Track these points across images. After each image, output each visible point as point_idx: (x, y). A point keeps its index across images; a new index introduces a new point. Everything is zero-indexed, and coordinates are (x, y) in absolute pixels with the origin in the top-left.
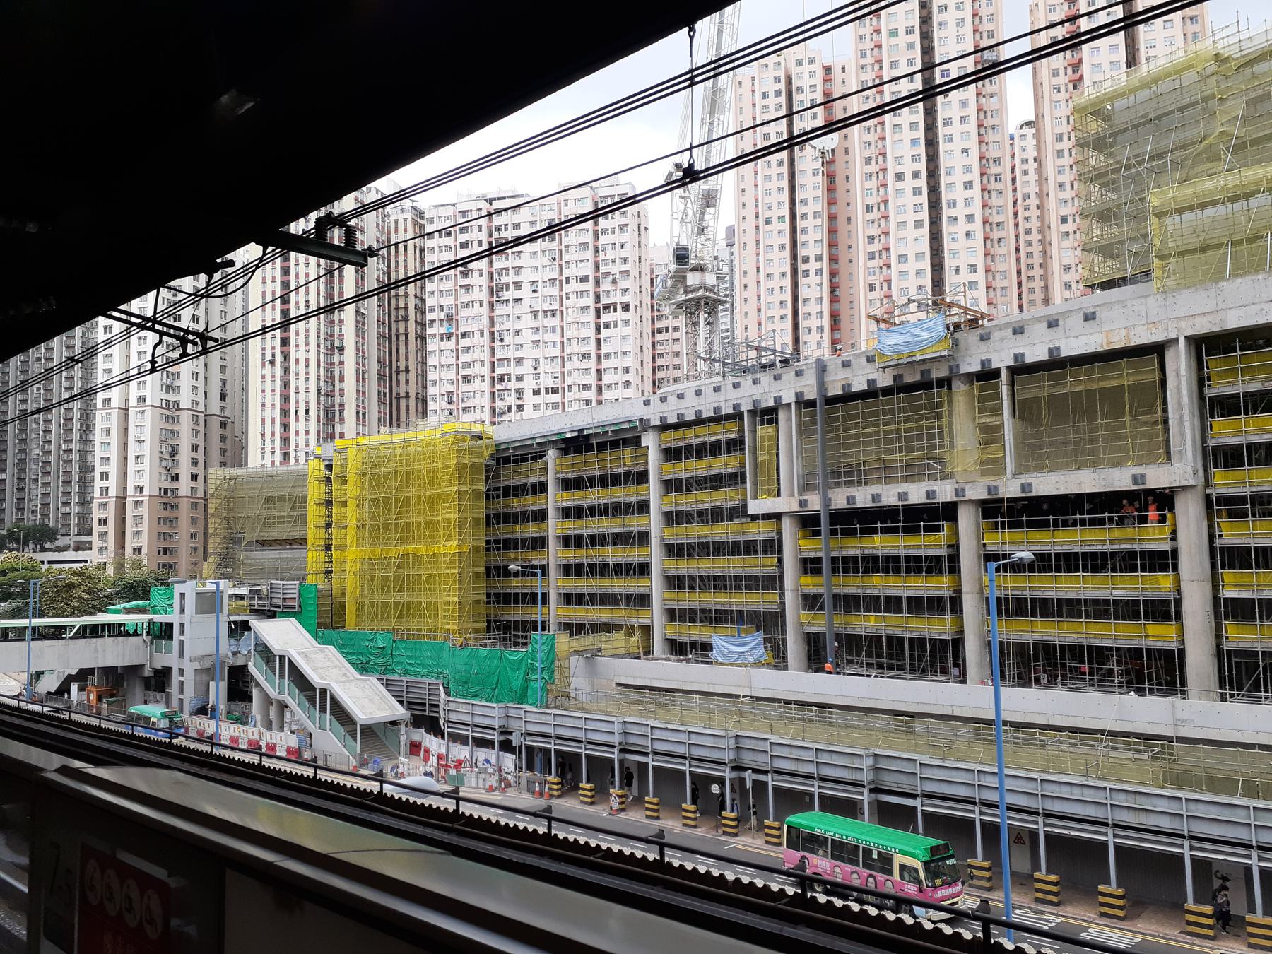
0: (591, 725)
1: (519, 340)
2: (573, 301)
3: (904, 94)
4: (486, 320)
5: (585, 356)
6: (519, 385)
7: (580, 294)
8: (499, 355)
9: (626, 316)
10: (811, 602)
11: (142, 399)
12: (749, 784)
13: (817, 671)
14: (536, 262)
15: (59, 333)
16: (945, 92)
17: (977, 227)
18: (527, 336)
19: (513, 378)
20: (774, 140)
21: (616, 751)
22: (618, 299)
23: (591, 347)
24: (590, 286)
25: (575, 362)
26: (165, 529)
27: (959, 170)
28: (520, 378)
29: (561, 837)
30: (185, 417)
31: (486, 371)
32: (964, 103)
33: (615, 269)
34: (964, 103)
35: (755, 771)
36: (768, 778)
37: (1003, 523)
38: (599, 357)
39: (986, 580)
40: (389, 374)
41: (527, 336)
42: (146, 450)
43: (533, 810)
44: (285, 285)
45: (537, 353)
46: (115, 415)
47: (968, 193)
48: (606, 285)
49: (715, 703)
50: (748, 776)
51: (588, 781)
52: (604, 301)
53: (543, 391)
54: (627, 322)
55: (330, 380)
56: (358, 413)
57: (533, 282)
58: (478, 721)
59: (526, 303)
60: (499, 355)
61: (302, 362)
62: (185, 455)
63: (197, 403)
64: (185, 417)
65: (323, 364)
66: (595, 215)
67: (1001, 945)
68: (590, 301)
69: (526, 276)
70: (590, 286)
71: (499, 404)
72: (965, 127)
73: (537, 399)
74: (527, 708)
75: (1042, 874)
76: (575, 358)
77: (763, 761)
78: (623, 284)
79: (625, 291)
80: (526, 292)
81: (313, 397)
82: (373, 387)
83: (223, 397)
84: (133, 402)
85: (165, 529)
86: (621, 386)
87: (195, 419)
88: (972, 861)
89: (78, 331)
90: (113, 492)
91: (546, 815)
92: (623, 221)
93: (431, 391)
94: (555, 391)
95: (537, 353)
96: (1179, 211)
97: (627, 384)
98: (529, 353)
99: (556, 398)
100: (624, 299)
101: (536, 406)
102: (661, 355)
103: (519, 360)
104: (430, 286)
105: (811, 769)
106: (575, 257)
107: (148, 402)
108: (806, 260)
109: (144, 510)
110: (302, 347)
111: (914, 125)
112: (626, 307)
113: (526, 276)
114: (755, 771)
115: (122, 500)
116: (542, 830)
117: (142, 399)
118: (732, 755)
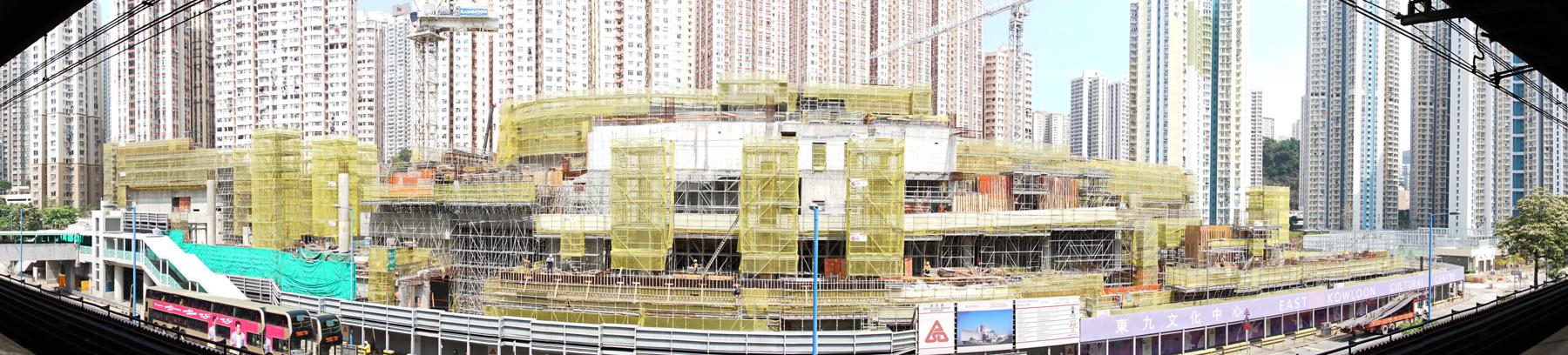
2: (310, 42)
5: (317, 76)
8: (260, 74)
22: (339, 40)
23: (321, 69)
24: (321, 32)
25: (309, 79)
31: (252, 84)
33: (337, 23)
36: (529, 345)
39: (995, 39)
40: (192, 88)
42: (56, 138)
48: (332, 32)
52: (331, 41)
55: (157, 93)
60: (260, 74)
62: (75, 139)
68: (321, 41)
70: (321, 32)
71: (261, 106)
78: (343, 31)
82: (182, 95)
83: (96, 106)
93: (217, 97)
99: (298, 101)
109: (56, 172)
112: (344, 46)
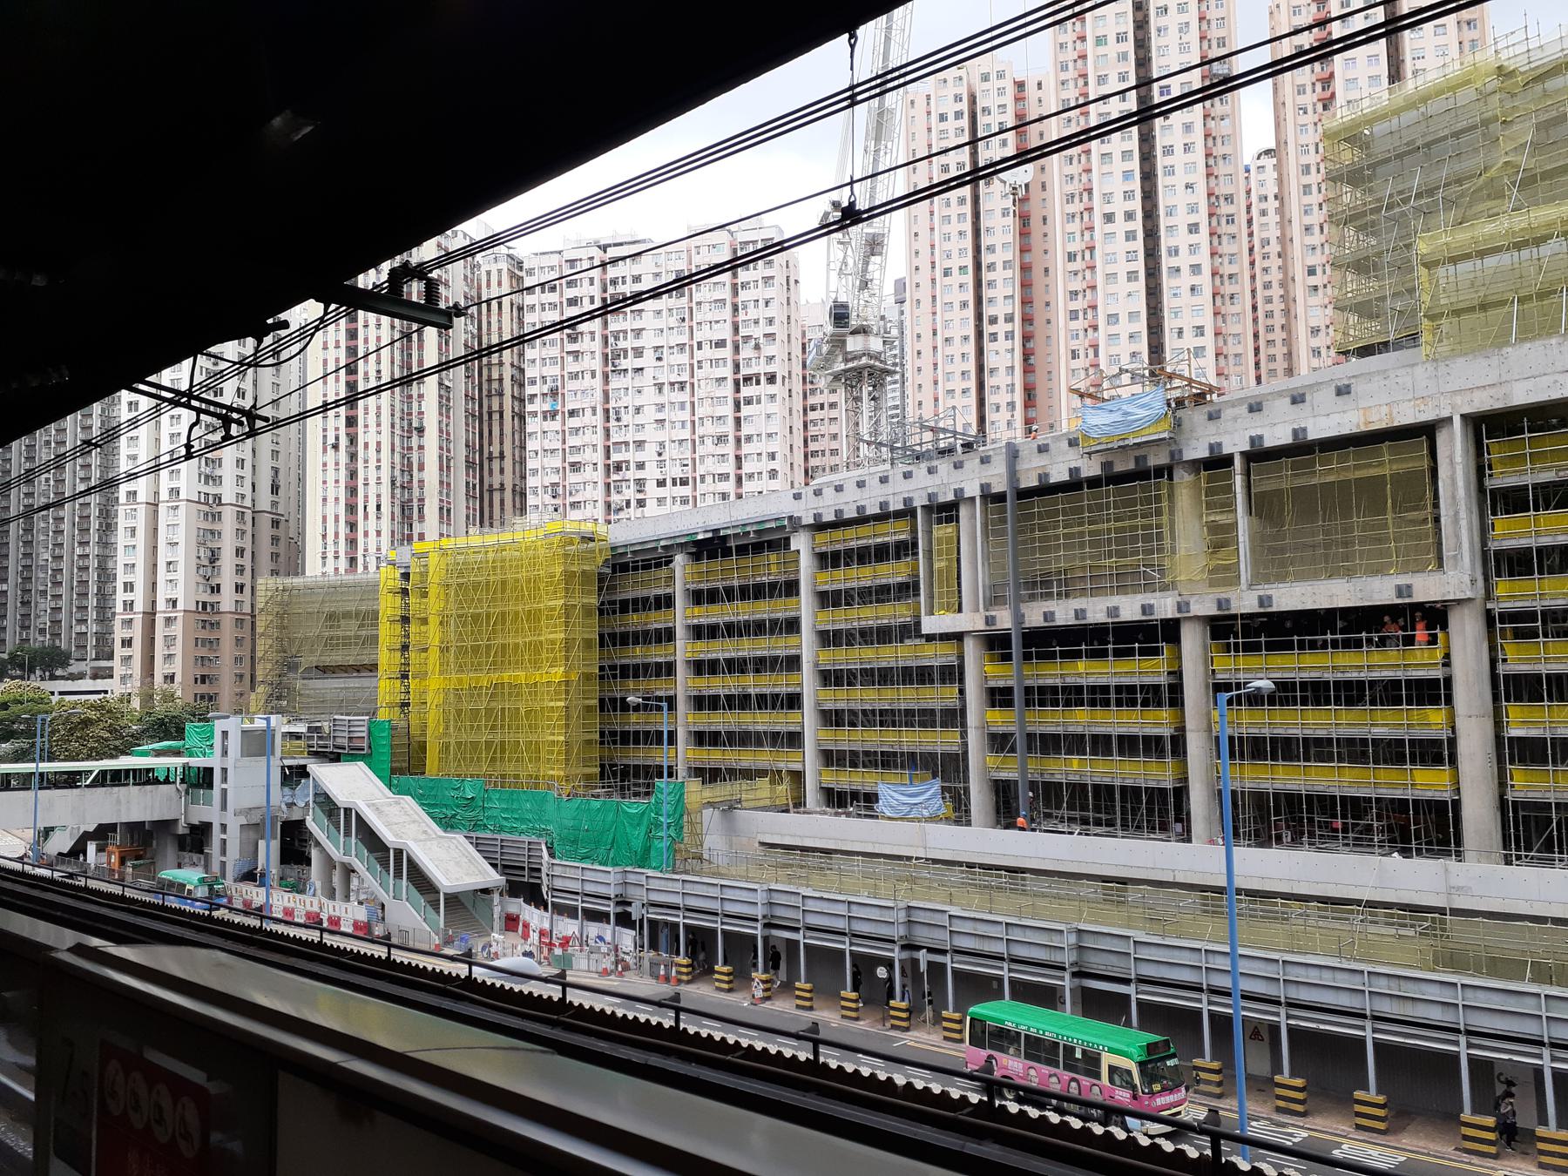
0: (729, 894)
1: (639, 419)
2: (706, 371)
3: (1115, 116)
4: (599, 395)
5: (721, 439)
6: (640, 475)
7: (715, 362)
8: (615, 438)
9: (772, 389)
10: (999, 742)
11: (175, 492)
12: (923, 967)
13: (1007, 827)
14: (661, 323)
15: (73, 411)
16: (1164, 114)
17: (1205, 279)
18: (650, 414)
19: (632, 466)
20: (954, 173)
21: (759, 926)
22: (761, 368)
23: (729, 428)
24: (727, 352)
25: (709, 446)
26: (203, 652)
27: (1182, 210)
28: (641, 466)
29: (691, 1032)
30: (229, 514)
31: (599, 457)
32: (1188, 127)
33: (758, 332)
34: (1188, 127)
35: (930, 950)
36: (947, 959)
37: (1236, 644)
38: (738, 440)
39: (1215, 714)
40: (480, 461)
41: (650, 414)
42: (180, 555)
43: (657, 999)
44: (352, 351)
45: (662, 435)
46: (142, 511)
47: (1194, 239)
48: (747, 352)
49: (881, 866)
50: (923, 956)
51: (725, 963)
52: (744, 371)
53: (669, 482)
54: (773, 397)
55: (407, 468)
56: (441, 509)
57: (657, 348)
58: (590, 888)
59: (648, 373)
60: (615, 438)
61: (372, 447)
62: (228, 561)
63: (243, 496)
64: (229, 514)
65: (398, 449)
66: (733, 265)
67: (1234, 1164)
68: (727, 371)
69: (648, 340)
70: (727, 352)
71: (615, 498)
72: (1190, 157)
73: (662, 492)
74: (650, 873)
75: (1284, 1077)
76: (708, 441)
77: (940, 938)
78: (768, 350)
79: (771, 359)
80: (648, 359)
81: (385, 490)
82: (460, 477)
83: (275, 489)
84: (164, 495)
85: (203, 652)
86: (765, 476)
87: (241, 516)
88: (1198, 1062)
89: (96, 407)
90: (139, 607)
91: (673, 1004)
92: (768, 272)
93: (531, 482)
94: (684, 482)
95: (662, 435)
96: (1454, 260)
97: (773, 474)
98: (651, 435)
99: (686, 491)
100: (770, 369)
101: (661, 501)
102: (815, 438)
103: (640, 444)
104: (530, 353)
105: (1000, 948)
106: (709, 317)
107: (183, 496)
108: (993, 320)
109: (177, 629)
110: (373, 428)
111: (1126, 155)
112: (771, 379)
113: (648, 340)
114: (930, 950)
115: (150, 616)
116: (668, 1023)
117: (175, 492)
118: (902, 931)
